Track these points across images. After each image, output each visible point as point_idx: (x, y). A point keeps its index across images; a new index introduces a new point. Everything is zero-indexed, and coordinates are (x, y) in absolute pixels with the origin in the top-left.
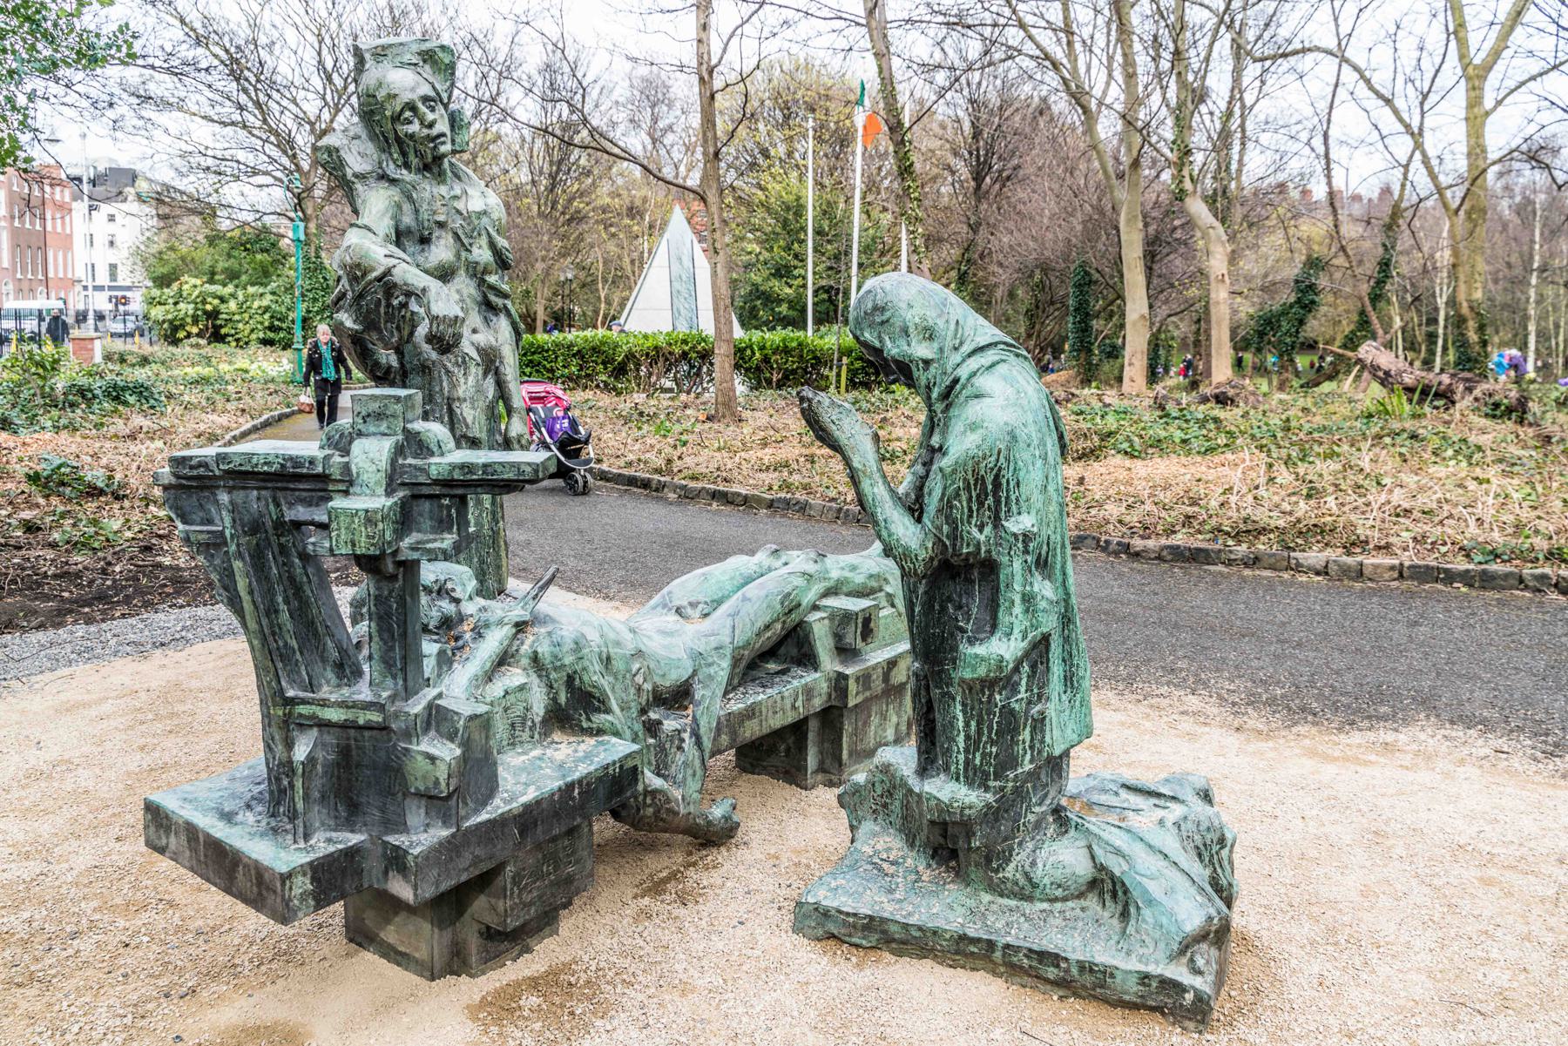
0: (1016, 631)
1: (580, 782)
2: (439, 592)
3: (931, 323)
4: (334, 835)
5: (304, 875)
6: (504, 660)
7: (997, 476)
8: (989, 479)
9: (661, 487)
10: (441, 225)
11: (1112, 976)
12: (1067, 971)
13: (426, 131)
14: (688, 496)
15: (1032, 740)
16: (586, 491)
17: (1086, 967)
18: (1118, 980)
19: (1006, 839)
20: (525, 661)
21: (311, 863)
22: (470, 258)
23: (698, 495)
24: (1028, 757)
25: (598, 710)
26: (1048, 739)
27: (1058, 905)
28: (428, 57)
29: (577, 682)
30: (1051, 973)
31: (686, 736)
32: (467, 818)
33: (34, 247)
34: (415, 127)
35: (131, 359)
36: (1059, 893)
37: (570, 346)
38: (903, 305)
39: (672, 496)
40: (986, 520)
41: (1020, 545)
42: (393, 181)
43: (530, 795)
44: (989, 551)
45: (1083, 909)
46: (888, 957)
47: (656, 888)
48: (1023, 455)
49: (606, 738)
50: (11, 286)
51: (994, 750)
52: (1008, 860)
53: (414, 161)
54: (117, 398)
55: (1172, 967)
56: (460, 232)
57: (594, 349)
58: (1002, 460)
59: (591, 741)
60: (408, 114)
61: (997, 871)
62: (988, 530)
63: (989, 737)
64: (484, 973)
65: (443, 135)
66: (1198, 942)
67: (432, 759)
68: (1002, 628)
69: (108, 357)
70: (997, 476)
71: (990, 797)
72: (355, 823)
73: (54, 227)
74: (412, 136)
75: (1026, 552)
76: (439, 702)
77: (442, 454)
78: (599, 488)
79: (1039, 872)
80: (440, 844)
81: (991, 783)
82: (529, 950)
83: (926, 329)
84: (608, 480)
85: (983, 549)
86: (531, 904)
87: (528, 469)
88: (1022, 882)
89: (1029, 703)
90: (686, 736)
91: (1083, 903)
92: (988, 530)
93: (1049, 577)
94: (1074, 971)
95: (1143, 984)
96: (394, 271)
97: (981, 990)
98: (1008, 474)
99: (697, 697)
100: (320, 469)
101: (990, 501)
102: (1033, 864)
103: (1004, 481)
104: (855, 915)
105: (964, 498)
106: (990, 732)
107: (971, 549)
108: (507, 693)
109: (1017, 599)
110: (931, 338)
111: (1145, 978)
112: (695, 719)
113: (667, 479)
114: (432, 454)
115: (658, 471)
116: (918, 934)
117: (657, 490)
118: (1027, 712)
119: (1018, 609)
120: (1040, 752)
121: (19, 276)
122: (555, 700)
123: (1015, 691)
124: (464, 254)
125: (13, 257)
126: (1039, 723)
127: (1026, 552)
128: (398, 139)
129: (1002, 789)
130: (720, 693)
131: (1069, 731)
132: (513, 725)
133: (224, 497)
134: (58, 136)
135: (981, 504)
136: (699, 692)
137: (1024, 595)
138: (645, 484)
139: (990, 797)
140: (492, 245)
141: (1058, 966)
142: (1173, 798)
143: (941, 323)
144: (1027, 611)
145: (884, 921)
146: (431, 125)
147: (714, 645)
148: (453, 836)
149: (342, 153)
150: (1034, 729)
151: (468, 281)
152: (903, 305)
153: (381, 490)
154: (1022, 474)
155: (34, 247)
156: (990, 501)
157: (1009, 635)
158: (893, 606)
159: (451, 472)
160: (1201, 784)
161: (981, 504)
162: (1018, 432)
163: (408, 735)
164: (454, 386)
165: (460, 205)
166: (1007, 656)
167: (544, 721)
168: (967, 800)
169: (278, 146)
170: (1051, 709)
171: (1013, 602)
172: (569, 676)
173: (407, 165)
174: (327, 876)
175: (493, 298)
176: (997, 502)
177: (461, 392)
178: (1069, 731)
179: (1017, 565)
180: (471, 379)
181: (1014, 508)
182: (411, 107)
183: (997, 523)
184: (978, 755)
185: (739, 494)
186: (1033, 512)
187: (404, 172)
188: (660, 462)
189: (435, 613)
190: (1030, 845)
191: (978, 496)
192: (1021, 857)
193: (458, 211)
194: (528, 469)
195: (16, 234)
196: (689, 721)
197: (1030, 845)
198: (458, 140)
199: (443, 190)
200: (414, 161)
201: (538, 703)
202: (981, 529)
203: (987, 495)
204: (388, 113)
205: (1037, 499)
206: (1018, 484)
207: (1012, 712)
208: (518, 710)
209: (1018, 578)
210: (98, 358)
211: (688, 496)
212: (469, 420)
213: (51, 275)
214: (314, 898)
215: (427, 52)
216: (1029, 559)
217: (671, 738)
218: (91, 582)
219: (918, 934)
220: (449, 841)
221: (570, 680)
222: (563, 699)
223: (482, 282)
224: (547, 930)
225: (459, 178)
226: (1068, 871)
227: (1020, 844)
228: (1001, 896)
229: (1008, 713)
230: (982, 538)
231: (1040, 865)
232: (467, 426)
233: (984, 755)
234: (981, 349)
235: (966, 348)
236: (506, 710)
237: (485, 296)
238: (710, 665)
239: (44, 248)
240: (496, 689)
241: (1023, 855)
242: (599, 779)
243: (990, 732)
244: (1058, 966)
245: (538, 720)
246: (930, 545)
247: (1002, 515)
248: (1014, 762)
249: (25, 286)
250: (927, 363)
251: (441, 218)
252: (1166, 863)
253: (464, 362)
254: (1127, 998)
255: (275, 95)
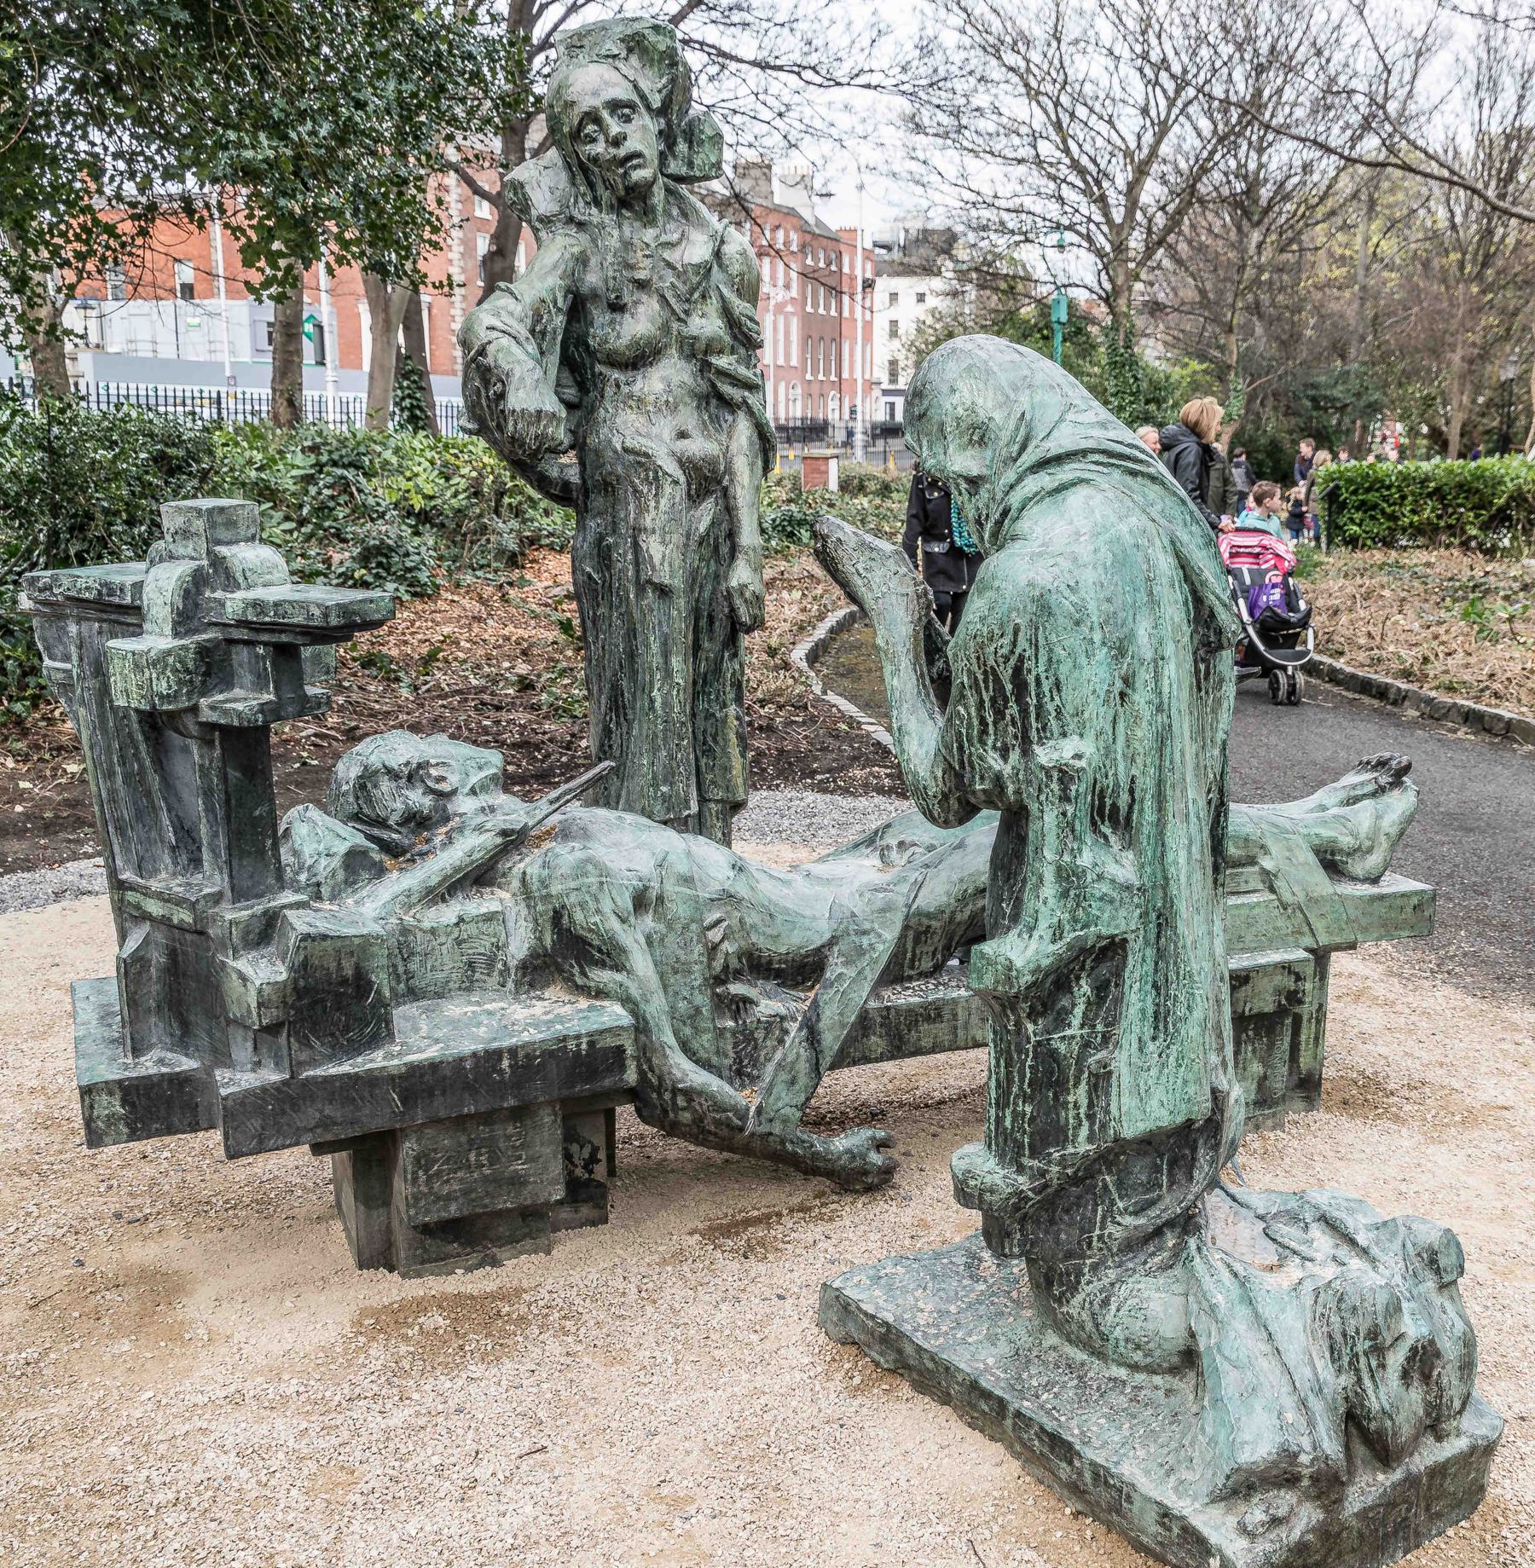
0: (1043, 924)
1: (513, 1051)
2: (410, 778)
3: (982, 416)
4: (169, 1055)
5: (111, 1094)
6: (481, 876)
7: (1018, 671)
8: (1006, 674)
9: (1401, 698)
10: (642, 285)
11: (1129, 1499)
12: (1080, 1474)
13: (613, 151)
14: (1435, 714)
15: (1091, 1105)
16: (1292, 699)
17: (1100, 1475)
18: (1136, 1508)
19: (1069, 1255)
20: (516, 884)
21: (120, 1082)
22: (685, 331)
23: (1445, 716)
24: (1084, 1132)
25: (602, 965)
26: (1113, 1108)
27: (1140, 1377)
28: (636, 44)
29: (565, 920)
30: (1064, 1470)
31: (793, 1027)
32: (313, 1063)
33: (827, 339)
34: (599, 148)
35: (872, 486)
36: (1138, 1357)
37: (1425, 481)
38: (945, 389)
39: (1412, 713)
40: (1010, 740)
41: (1055, 786)
42: (581, 225)
43: (432, 1053)
44: (1018, 792)
45: (1169, 1392)
46: (905, 1390)
47: (718, 1232)
48: (1065, 641)
49: (606, 1003)
50: (799, 390)
51: (1028, 1109)
52: (1074, 1288)
53: (605, 195)
54: (791, 535)
55: (1217, 1511)
56: (669, 295)
57: (1460, 486)
58: (1022, 643)
59: (583, 1003)
60: (590, 128)
61: (1059, 1300)
62: (1015, 756)
63: (1021, 1088)
64: (420, 1276)
65: (639, 155)
66: (1279, 1486)
67: (244, 979)
68: (1026, 918)
69: (845, 486)
70: (1018, 671)
71: (1023, 1182)
72: (186, 1047)
73: (852, 311)
74: (595, 160)
75: (1065, 798)
76: (287, 912)
77: (249, 587)
78: (1313, 692)
79: (1109, 1318)
80: (264, 1089)
81: (1027, 1161)
82: (495, 1263)
83: (974, 427)
84: (1338, 683)
85: (1011, 789)
86: (449, 1198)
87: (317, 612)
88: (1089, 1326)
89: (1086, 1045)
90: (793, 1027)
91: (1175, 1383)
92: (1015, 756)
93: (1130, 844)
94: (1088, 1476)
95: (1163, 1525)
96: (491, 349)
97: (982, 1466)
98: (1036, 669)
99: (829, 974)
100: (128, 600)
101: (1013, 709)
102: (1105, 1303)
103: (1031, 679)
104: (873, 1317)
105: (972, 701)
106: (1022, 1081)
107: (987, 786)
108: (461, 920)
109: (1049, 874)
110: (982, 442)
111: (1165, 1515)
112: (815, 1004)
113: (1414, 687)
114: (238, 587)
115: (1407, 674)
116: (930, 1365)
117: (1395, 703)
118: (1080, 1060)
119: (1049, 890)
120: (1103, 1126)
121: (809, 377)
122: (540, 939)
123: (1061, 1021)
124: (675, 325)
125: (803, 351)
126: (1101, 1081)
127: (1065, 798)
128: (581, 165)
129: (1043, 1173)
130: (872, 975)
131: (1154, 1103)
132: (471, 965)
133: (73, 629)
134: (832, 188)
135: (999, 714)
136: (835, 967)
137: (1059, 869)
138: (1382, 692)
139: (1023, 1182)
140: (726, 312)
141: (1070, 1463)
142: (1365, 1251)
143: (998, 416)
144: (1064, 895)
145: (901, 1335)
146: (617, 142)
147: (879, 905)
148: (285, 1083)
149: (527, 189)
150: (1094, 1089)
151: (682, 364)
152: (945, 389)
153: (168, 629)
154: (1064, 669)
155: (827, 339)
156: (1013, 709)
157: (1031, 929)
158: (1272, 890)
159: (245, 610)
160: (1429, 1235)
161: (999, 714)
162: (1053, 599)
163: (223, 945)
164: (642, 510)
165: (671, 256)
166: (1019, 963)
167: (524, 966)
168: (988, 1179)
169: (1084, 192)
170: (1122, 1061)
171: (1041, 879)
172: (555, 911)
173: (596, 202)
174: (144, 1101)
175: (726, 389)
176: (1024, 712)
177: (648, 521)
178: (1154, 1103)
179: (1050, 818)
180: (663, 502)
181: (1053, 724)
182: (593, 117)
183: (1026, 752)
184: (1008, 1112)
185: (1499, 718)
186: (1090, 735)
187: (594, 211)
188: (1410, 657)
189: (399, 805)
190: (1112, 1274)
191: (993, 700)
192: (1090, 1288)
193: (669, 265)
194: (317, 612)
195: (807, 320)
196: (804, 1007)
197: (1112, 1274)
198: (698, 161)
199: (649, 235)
200: (605, 195)
201: (519, 944)
202: (1004, 753)
203: (1006, 700)
204: (566, 129)
205: (1098, 714)
206: (1058, 685)
207: (1053, 1054)
208: (484, 946)
209: (1051, 840)
210: (833, 485)
211: (1435, 714)
212: (657, 559)
213: (845, 375)
214: (127, 1125)
215: (632, 37)
216: (1070, 809)
217: (768, 1027)
218: (548, 756)
219: (930, 1365)
220: (279, 1088)
221: (557, 916)
222: (548, 942)
223: (705, 366)
224: (528, 1243)
225: (685, 215)
226: (1150, 1326)
227: (1094, 1268)
228: (1070, 1341)
229: (1047, 1055)
230: (1007, 770)
231: (1113, 1307)
232: (653, 568)
233: (1015, 1114)
234: (1058, 460)
235: (1028, 458)
236: (459, 942)
237: (713, 385)
238: (865, 933)
239: (838, 340)
240: (447, 914)
241: (1097, 1285)
242: (549, 1054)
243: (1022, 1081)
244: (1070, 1463)
245: (513, 963)
246: (940, 774)
247: (1033, 734)
248: (1060, 1135)
249: (815, 389)
250: (974, 482)
251: (641, 275)
252: (1266, 1348)
253: (656, 478)
254: (1145, 1539)
255: (1082, 112)
